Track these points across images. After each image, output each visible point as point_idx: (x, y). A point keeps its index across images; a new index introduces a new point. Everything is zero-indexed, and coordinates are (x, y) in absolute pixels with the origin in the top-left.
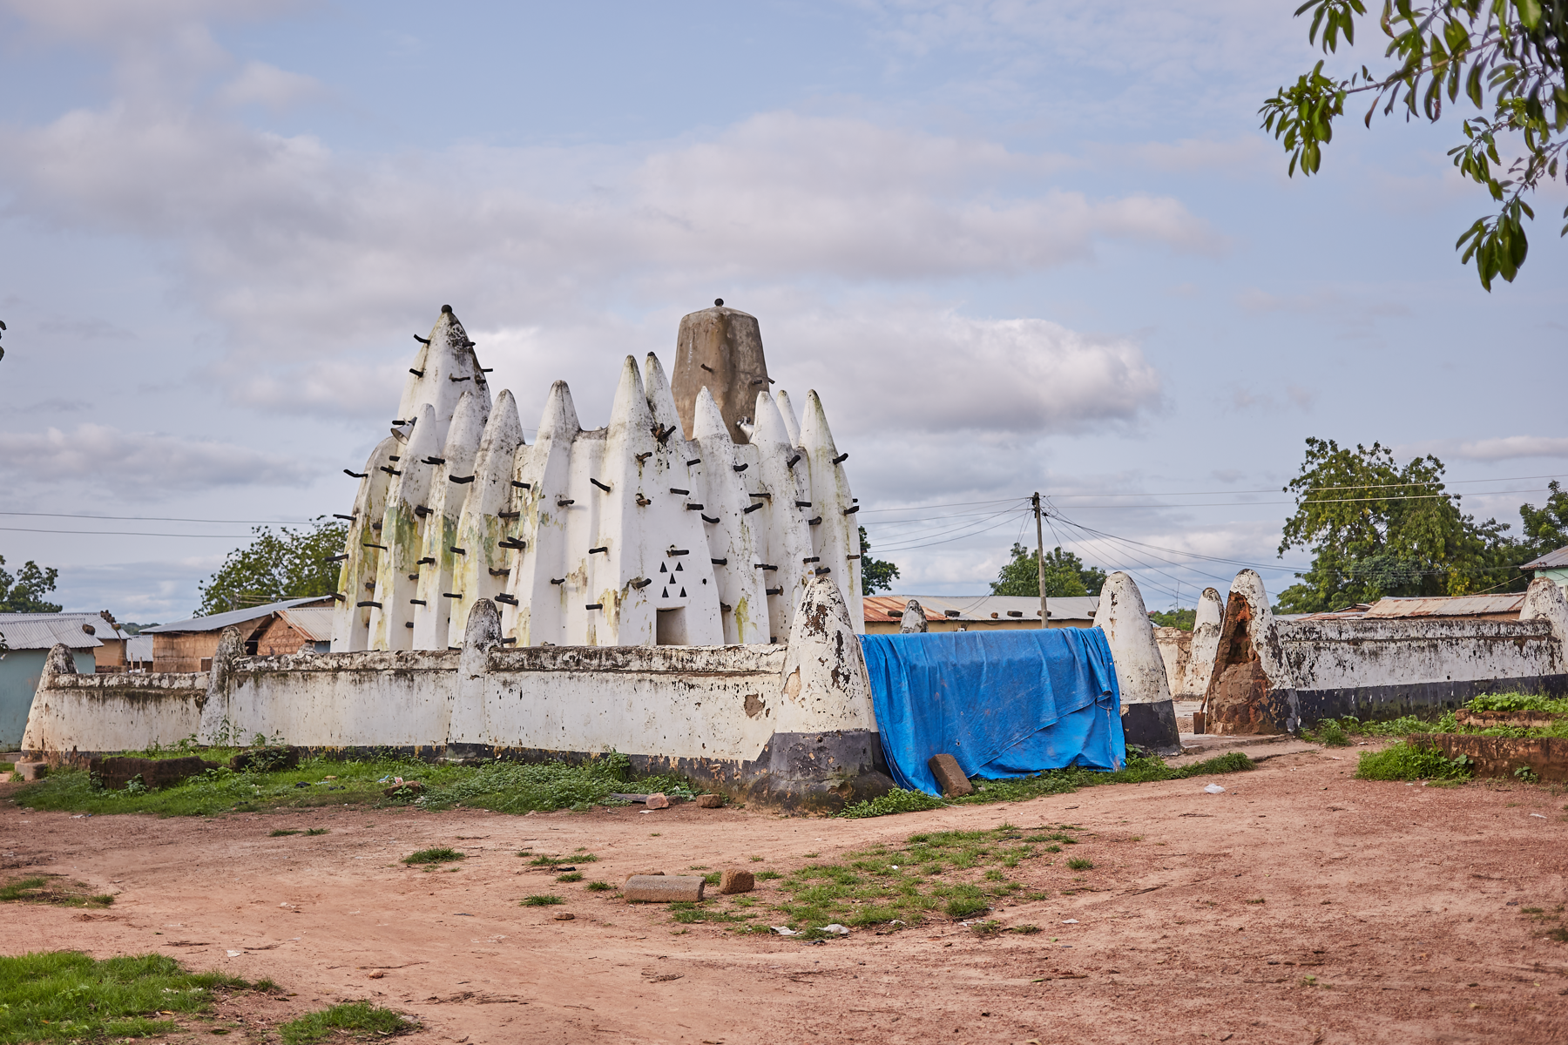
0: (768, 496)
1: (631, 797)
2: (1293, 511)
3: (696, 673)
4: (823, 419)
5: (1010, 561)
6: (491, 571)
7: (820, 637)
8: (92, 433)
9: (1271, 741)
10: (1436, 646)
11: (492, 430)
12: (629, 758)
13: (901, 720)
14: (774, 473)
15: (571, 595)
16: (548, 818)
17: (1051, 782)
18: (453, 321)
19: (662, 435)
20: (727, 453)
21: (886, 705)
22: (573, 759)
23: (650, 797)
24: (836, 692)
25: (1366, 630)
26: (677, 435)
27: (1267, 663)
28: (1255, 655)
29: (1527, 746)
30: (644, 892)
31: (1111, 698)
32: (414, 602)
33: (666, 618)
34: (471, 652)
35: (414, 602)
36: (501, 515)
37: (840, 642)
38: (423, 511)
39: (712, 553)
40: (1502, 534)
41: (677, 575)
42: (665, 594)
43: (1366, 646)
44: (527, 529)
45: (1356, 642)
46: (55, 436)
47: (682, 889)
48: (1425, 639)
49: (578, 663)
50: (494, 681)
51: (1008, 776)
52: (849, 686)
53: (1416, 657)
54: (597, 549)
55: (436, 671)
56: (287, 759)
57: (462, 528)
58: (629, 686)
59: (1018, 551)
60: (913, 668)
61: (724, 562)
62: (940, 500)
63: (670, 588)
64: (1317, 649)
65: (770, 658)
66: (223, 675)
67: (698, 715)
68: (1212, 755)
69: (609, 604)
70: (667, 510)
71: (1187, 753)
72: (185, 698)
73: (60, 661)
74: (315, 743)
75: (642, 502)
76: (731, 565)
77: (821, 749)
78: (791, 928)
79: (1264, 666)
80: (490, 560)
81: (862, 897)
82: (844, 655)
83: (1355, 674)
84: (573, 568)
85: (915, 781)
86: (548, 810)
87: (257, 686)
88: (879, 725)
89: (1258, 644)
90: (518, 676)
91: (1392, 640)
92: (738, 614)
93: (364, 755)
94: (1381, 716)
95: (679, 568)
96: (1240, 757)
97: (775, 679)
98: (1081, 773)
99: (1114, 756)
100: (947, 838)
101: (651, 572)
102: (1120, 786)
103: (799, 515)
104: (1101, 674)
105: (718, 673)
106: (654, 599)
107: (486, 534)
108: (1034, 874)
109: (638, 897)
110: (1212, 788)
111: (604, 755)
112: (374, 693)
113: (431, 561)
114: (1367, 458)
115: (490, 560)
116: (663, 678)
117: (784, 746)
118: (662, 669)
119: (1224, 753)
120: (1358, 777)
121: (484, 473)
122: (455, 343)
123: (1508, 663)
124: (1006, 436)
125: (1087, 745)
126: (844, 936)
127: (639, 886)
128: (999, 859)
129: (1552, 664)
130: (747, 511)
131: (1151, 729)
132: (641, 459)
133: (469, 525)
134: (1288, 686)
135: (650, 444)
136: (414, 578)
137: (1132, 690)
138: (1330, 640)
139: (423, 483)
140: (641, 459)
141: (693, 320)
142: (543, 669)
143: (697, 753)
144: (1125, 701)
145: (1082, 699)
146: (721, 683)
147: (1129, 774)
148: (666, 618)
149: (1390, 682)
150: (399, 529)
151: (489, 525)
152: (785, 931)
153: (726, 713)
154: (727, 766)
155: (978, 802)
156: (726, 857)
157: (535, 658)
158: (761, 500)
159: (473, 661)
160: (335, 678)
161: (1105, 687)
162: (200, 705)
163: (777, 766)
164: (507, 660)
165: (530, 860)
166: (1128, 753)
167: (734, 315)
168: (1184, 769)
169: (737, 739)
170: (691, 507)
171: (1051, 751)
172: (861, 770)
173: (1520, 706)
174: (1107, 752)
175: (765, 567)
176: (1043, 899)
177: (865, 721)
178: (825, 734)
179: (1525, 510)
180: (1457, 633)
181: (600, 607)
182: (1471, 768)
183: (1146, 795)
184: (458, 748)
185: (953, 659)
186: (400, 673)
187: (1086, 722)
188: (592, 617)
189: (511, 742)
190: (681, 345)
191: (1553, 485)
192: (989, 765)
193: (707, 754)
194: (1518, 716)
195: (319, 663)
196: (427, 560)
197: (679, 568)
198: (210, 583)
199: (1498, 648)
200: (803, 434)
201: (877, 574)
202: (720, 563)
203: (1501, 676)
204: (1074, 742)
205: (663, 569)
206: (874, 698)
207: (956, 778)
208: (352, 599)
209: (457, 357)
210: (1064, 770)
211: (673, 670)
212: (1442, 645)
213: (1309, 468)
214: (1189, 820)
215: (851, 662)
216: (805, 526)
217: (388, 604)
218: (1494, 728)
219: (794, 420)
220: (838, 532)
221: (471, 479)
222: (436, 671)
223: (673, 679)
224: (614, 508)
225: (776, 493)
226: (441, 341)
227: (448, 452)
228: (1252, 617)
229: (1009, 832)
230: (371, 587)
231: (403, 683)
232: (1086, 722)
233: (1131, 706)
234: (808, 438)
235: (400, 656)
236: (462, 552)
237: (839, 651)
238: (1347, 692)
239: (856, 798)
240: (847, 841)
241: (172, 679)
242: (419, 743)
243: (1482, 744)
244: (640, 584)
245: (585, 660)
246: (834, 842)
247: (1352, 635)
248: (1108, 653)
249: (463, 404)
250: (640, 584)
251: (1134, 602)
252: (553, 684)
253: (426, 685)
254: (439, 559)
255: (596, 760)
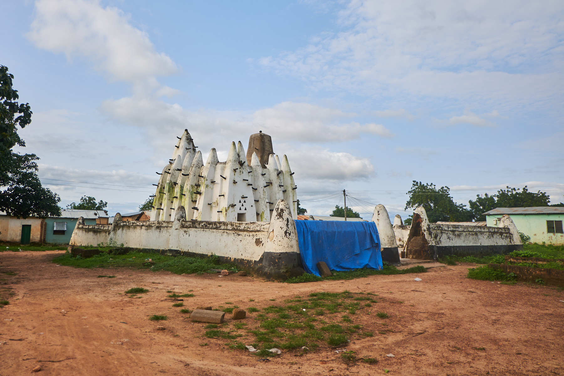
0: (271, 183)
1: (217, 270)
2: (409, 199)
3: (241, 230)
4: (288, 163)
5: (335, 209)
6: (192, 201)
7: (281, 220)
8: (122, 172)
9: (429, 262)
10: (477, 234)
11: (195, 161)
12: (219, 257)
13: (308, 249)
14: (273, 177)
15: (214, 208)
16: (187, 277)
17: (359, 273)
18: (188, 133)
19: (241, 164)
20: (260, 170)
21: (302, 243)
22: (202, 256)
23: (223, 271)
24: (286, 239)
25: (456, 228)
26: (246, 164)
27: (427, 236)
28: (423, 234)
29: (541, 271)
30: (199, 317)
31: (378, 245)
32: (171, 209)
33: (241, 217)
34: (176, 222)
35: (171, 209)
36: (196, 185)
37: (288, 222)
38: (175, 184)
39: (255, 198)
40: (464, 208)
41: (244, 204)
42: (240, 209)
43: (456, 233)
44: (202, 189)
45: (453, 231)
46: (114, 172)
47: (214, 317)
48: (473, 231)
49: (206, 226)
50: (182, 231)
51: (343, 270)
52: (290, 237)
53: (471, 237)
54: (222, 196)
55: (167, 227)
56: (124, 251)
57: (185, 189)
58: (220, 234)
59: (337, 207)
60: (312, 232)
61: (258, 201)
62: (319, 196)
63: (242, 208)
64: (442, 233)
65: (265, 227)
66: (115, 226)
67: (241, 244)
68: (409, 267)
69: (224, 211)
70: (240, 183)
71: (403, 265)
72: (106, 232)
73: (81, 221)
74: (135, 247)
75: (235, 182)
76: (260, 202)
77: (280, 258)
78: (255, 347)
79: (426, 237)
80: (192, 198)
81: (290, 327)
82: (289, 226)
83: (453, 242)
84: (214, 200)
85: (312, 270)
86: (189, 273)
87: (123, 230)
88: (300, 251)
89: (424, 230)
90: (189, 230)
91: (464, 231)
92: (261, 216)
93: (145, 251)
94: (464, 255)
95: (245, 202)
96: (422, 267)
97: (266, 233)
98: (367, 271)
99: (379, 265)
100: (325, 295)
101: (237, 202)
102: (382, 276)
103: (280, 189)
104: (375, 237)
105: (247, 231)
106: (237, 211)
107: (191, 190)
108: (364, 319)
109: (196, 319)
110: (417, 279)
111: (212, 256)
112: (151, 233)
113: (176, 197)
114: (429, 187)
115: (192, 198)
116: (230, 232)
117: (267, 256)
118: (231, 229)
119: (416, 265)
120: (469, 278)
121: (192, 173)
122: (188, 139)
123: (498, 241)
124: (336, 181)
125: (370, 261)
126: (279, 356)
127: (197, 315)
128: (346, 308)
129: (510, 241)
130: (265, 187)
131: (391, 256)
132: (235, 170)
133: (187, 187)
134: (434, 244)
135: (238, 166)
136: (172, 202)
137: (384, 243)
138: (446, 230)
139: (176, 176)
140: (235, 170)
141: (253, 136)
142: (196, 227)
143: (240, 257)
144: (383, 246)
145: (368, 245)
146: (248, 234)
147: (385, 271)
148: (241, 217)
149: (463, 245)
150: (169, 189)
151: (192, 188)
152: (252, 349)
153: (249, 244)
154: (249, 262)
155: (334, 279)
156: (240, 298)
157: (194, 224)
158: (269, 184)
159: (177, 225)
160: (141, 228)
161: (376, 241)
162: (109, 234)
163: (265, 263)
164: (188, 225)
165: (171, 294)
166: (383, 264)
167: (264, 135)
168: (403, 270)
169: (254, 254)
170: (249, 185)
171: (358, 262)
172: (294, 266)
173: (532, 255)
174: (376, 264)
175: (270, 203)
176: (371, 336)
177: (295, 249)
178: (282, 253)
179: (470, 202)
180: (483, 230)
181: (221, 212)
182: (516, 278)
183: (393, 280)
184: (171, 251)
185: (326, 230)
186: (158, 227)
187: (369, 253)
188: (219, 215)
189: (185, 250)
190: (250, 143)
191: (478, 196)
192: (337, 266)
193: (243, 257)
194: (531, 259)
195: (138, 224)
196: (175, 197)
197: (245, 202)
198: (141, 207)
199: (495, 236)
200: (282, 167)
201: (302, 211)
202: (257, 201)
203: (496, 245)
204: (365, 260)
205: (240, 202)
206: (299, 241)
207: (326, 270)
208: (156, 207)
209: (188, 143)
210: (362, 269)
211: (233, 229)
212: (479, 234)
213: (413, 188)
214: (417, 293)
215: (291, 229)
216: (281, 192)
217: (165, 209)
218: (521, 263)
219: (280, 163)
220: (291, 194)
221: (188, 175)
222: (167, 227)
223: (233, 232)
224: (227, 184)
225: (274, 182)
226: (184, 139)
227: (183, 168)
228: (422, 221)
229: (347, 295)
230: (161, 204)
231: (158, 230)
232: (369, 253)
233: (384, 248)
234: (283, 168)
235: (158, 223)
236: (185, 195)
237: (287, 225)
238: (451, 247)
239: (291, 276)
240: (286, 293)
241: (104, 227)
242: (161, 248)
243: (520, 269)
244: (233, 206)
245: (208, 225)
246: (282, 293)
247: (452, 229)
248: (377, 230)
249: (188, 154)
250: (233, 206)
251: (385, 214)
252: (198, 232)
253: (164, 231)
254: (179, 197)
255: (209, 257)
